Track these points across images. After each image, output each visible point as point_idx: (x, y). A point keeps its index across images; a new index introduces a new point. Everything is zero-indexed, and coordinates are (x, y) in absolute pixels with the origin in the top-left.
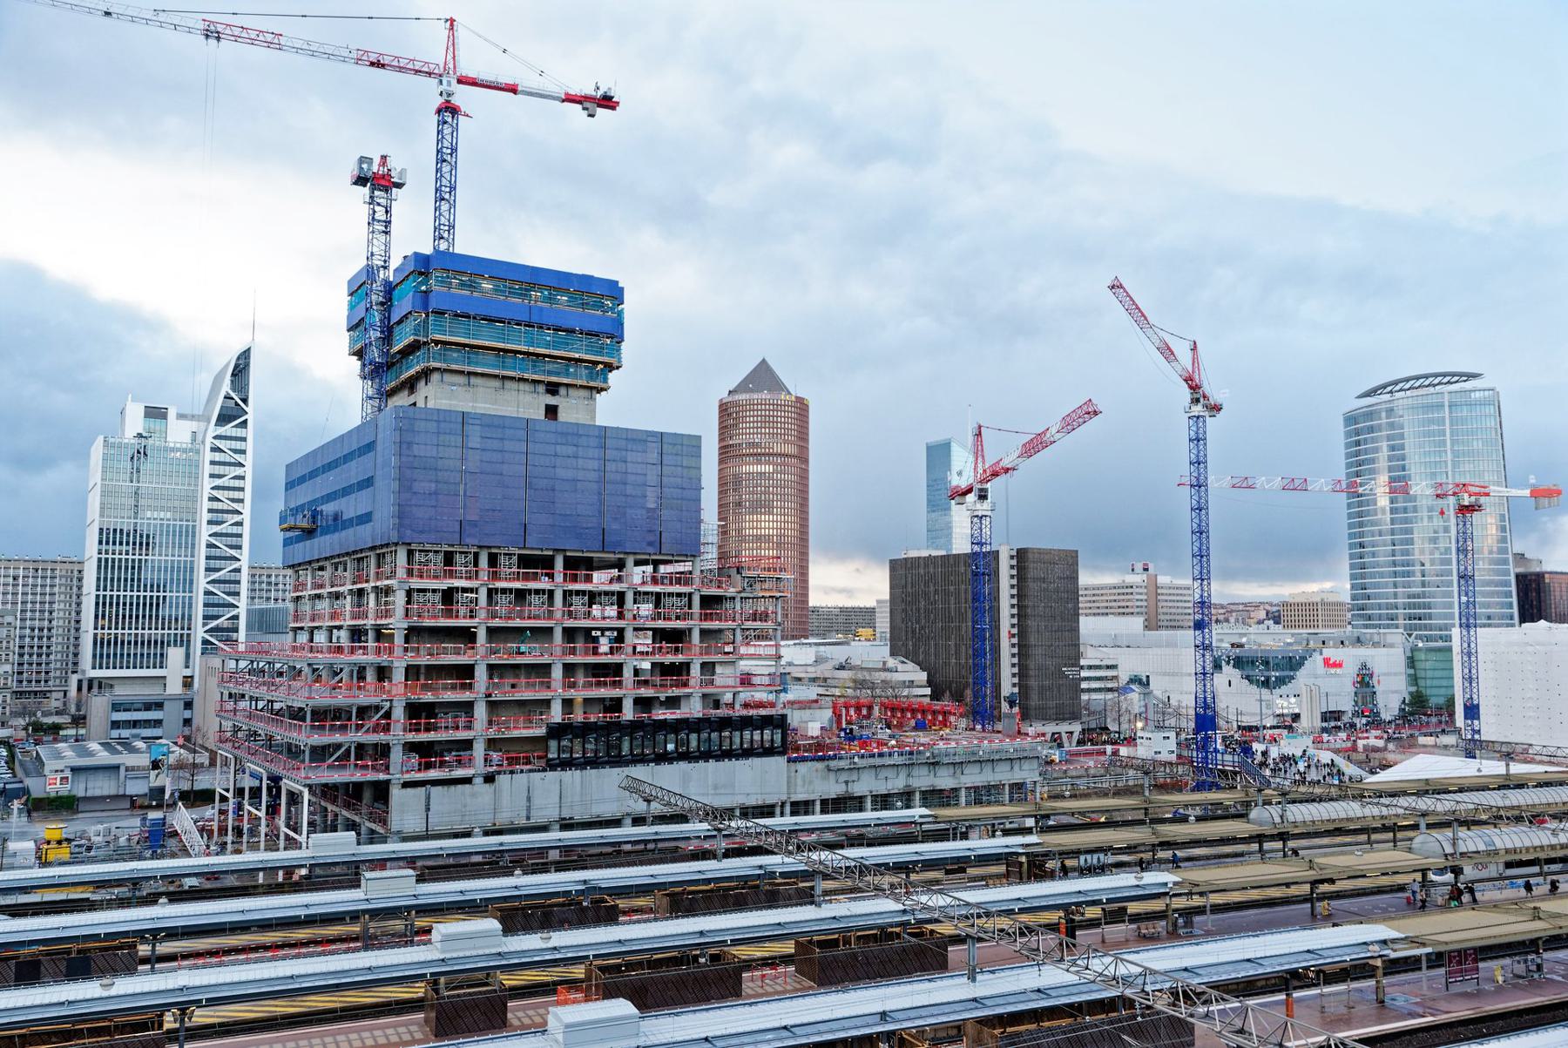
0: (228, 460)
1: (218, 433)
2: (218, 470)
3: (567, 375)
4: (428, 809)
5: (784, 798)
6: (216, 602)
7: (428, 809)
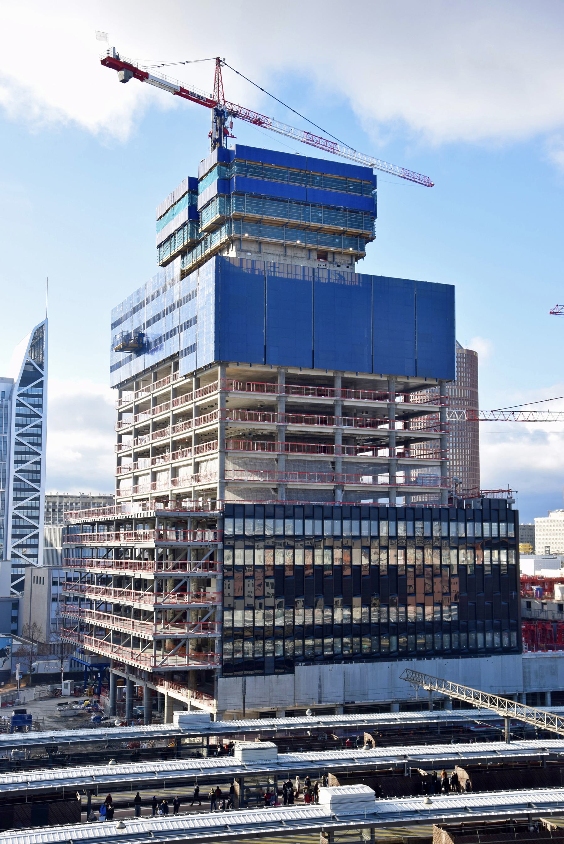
0: (29, 413)
1: (21, 392)
2: (22, 420)
3: (333, 245)
4: (244, 692)
5: (521, 690)
6: (21, 524)
7: (244, 692)
